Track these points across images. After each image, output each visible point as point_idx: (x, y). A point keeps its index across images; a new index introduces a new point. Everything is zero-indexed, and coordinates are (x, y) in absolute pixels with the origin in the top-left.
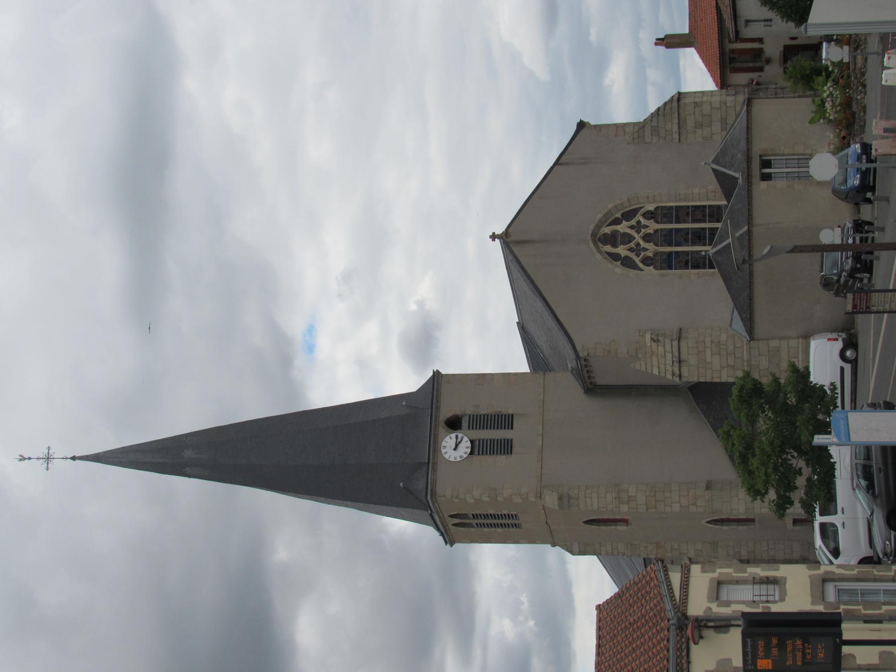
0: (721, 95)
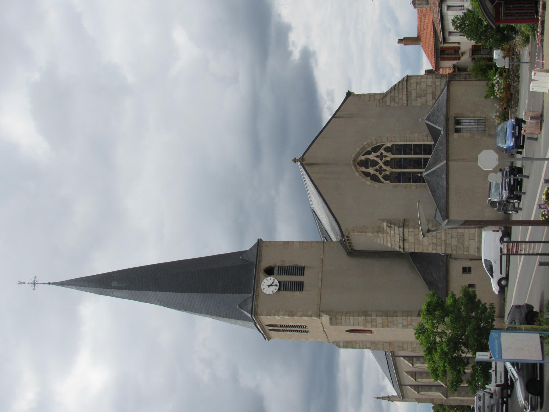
0: (432, 78)
